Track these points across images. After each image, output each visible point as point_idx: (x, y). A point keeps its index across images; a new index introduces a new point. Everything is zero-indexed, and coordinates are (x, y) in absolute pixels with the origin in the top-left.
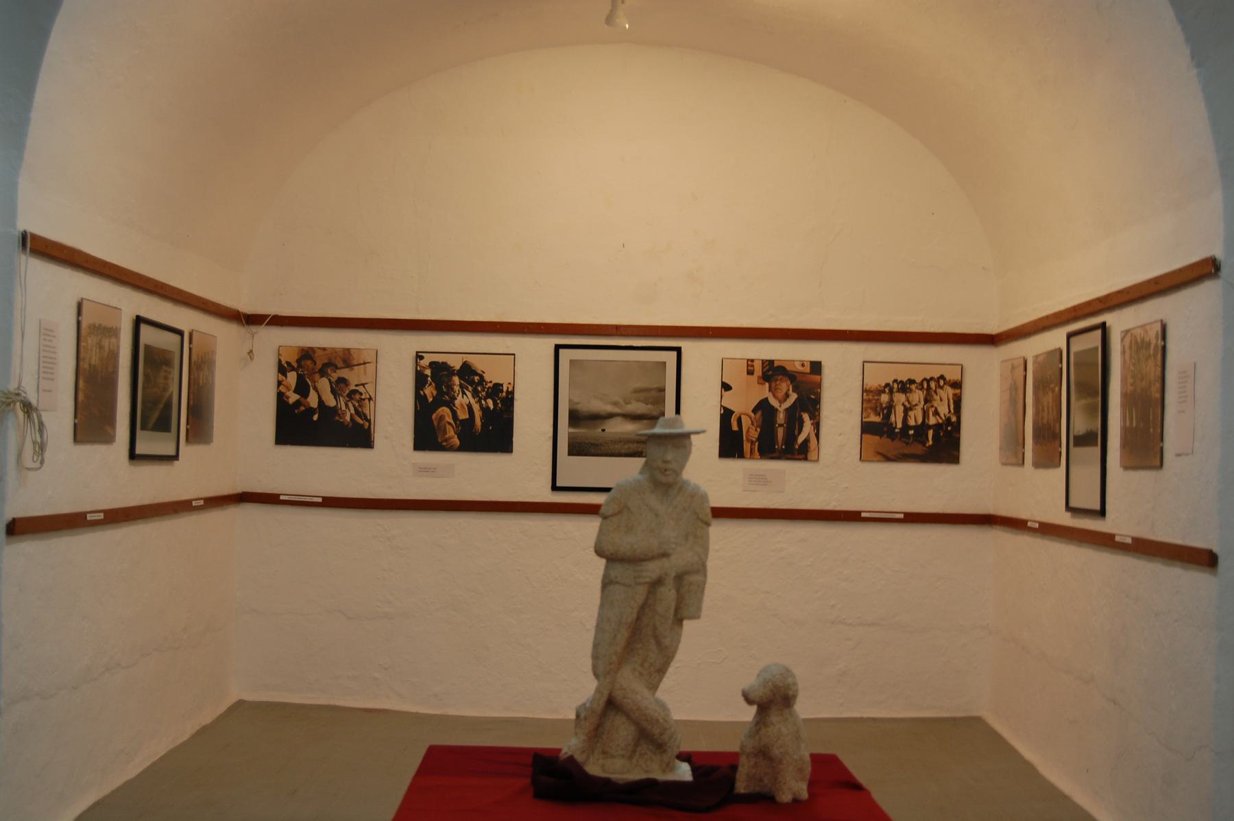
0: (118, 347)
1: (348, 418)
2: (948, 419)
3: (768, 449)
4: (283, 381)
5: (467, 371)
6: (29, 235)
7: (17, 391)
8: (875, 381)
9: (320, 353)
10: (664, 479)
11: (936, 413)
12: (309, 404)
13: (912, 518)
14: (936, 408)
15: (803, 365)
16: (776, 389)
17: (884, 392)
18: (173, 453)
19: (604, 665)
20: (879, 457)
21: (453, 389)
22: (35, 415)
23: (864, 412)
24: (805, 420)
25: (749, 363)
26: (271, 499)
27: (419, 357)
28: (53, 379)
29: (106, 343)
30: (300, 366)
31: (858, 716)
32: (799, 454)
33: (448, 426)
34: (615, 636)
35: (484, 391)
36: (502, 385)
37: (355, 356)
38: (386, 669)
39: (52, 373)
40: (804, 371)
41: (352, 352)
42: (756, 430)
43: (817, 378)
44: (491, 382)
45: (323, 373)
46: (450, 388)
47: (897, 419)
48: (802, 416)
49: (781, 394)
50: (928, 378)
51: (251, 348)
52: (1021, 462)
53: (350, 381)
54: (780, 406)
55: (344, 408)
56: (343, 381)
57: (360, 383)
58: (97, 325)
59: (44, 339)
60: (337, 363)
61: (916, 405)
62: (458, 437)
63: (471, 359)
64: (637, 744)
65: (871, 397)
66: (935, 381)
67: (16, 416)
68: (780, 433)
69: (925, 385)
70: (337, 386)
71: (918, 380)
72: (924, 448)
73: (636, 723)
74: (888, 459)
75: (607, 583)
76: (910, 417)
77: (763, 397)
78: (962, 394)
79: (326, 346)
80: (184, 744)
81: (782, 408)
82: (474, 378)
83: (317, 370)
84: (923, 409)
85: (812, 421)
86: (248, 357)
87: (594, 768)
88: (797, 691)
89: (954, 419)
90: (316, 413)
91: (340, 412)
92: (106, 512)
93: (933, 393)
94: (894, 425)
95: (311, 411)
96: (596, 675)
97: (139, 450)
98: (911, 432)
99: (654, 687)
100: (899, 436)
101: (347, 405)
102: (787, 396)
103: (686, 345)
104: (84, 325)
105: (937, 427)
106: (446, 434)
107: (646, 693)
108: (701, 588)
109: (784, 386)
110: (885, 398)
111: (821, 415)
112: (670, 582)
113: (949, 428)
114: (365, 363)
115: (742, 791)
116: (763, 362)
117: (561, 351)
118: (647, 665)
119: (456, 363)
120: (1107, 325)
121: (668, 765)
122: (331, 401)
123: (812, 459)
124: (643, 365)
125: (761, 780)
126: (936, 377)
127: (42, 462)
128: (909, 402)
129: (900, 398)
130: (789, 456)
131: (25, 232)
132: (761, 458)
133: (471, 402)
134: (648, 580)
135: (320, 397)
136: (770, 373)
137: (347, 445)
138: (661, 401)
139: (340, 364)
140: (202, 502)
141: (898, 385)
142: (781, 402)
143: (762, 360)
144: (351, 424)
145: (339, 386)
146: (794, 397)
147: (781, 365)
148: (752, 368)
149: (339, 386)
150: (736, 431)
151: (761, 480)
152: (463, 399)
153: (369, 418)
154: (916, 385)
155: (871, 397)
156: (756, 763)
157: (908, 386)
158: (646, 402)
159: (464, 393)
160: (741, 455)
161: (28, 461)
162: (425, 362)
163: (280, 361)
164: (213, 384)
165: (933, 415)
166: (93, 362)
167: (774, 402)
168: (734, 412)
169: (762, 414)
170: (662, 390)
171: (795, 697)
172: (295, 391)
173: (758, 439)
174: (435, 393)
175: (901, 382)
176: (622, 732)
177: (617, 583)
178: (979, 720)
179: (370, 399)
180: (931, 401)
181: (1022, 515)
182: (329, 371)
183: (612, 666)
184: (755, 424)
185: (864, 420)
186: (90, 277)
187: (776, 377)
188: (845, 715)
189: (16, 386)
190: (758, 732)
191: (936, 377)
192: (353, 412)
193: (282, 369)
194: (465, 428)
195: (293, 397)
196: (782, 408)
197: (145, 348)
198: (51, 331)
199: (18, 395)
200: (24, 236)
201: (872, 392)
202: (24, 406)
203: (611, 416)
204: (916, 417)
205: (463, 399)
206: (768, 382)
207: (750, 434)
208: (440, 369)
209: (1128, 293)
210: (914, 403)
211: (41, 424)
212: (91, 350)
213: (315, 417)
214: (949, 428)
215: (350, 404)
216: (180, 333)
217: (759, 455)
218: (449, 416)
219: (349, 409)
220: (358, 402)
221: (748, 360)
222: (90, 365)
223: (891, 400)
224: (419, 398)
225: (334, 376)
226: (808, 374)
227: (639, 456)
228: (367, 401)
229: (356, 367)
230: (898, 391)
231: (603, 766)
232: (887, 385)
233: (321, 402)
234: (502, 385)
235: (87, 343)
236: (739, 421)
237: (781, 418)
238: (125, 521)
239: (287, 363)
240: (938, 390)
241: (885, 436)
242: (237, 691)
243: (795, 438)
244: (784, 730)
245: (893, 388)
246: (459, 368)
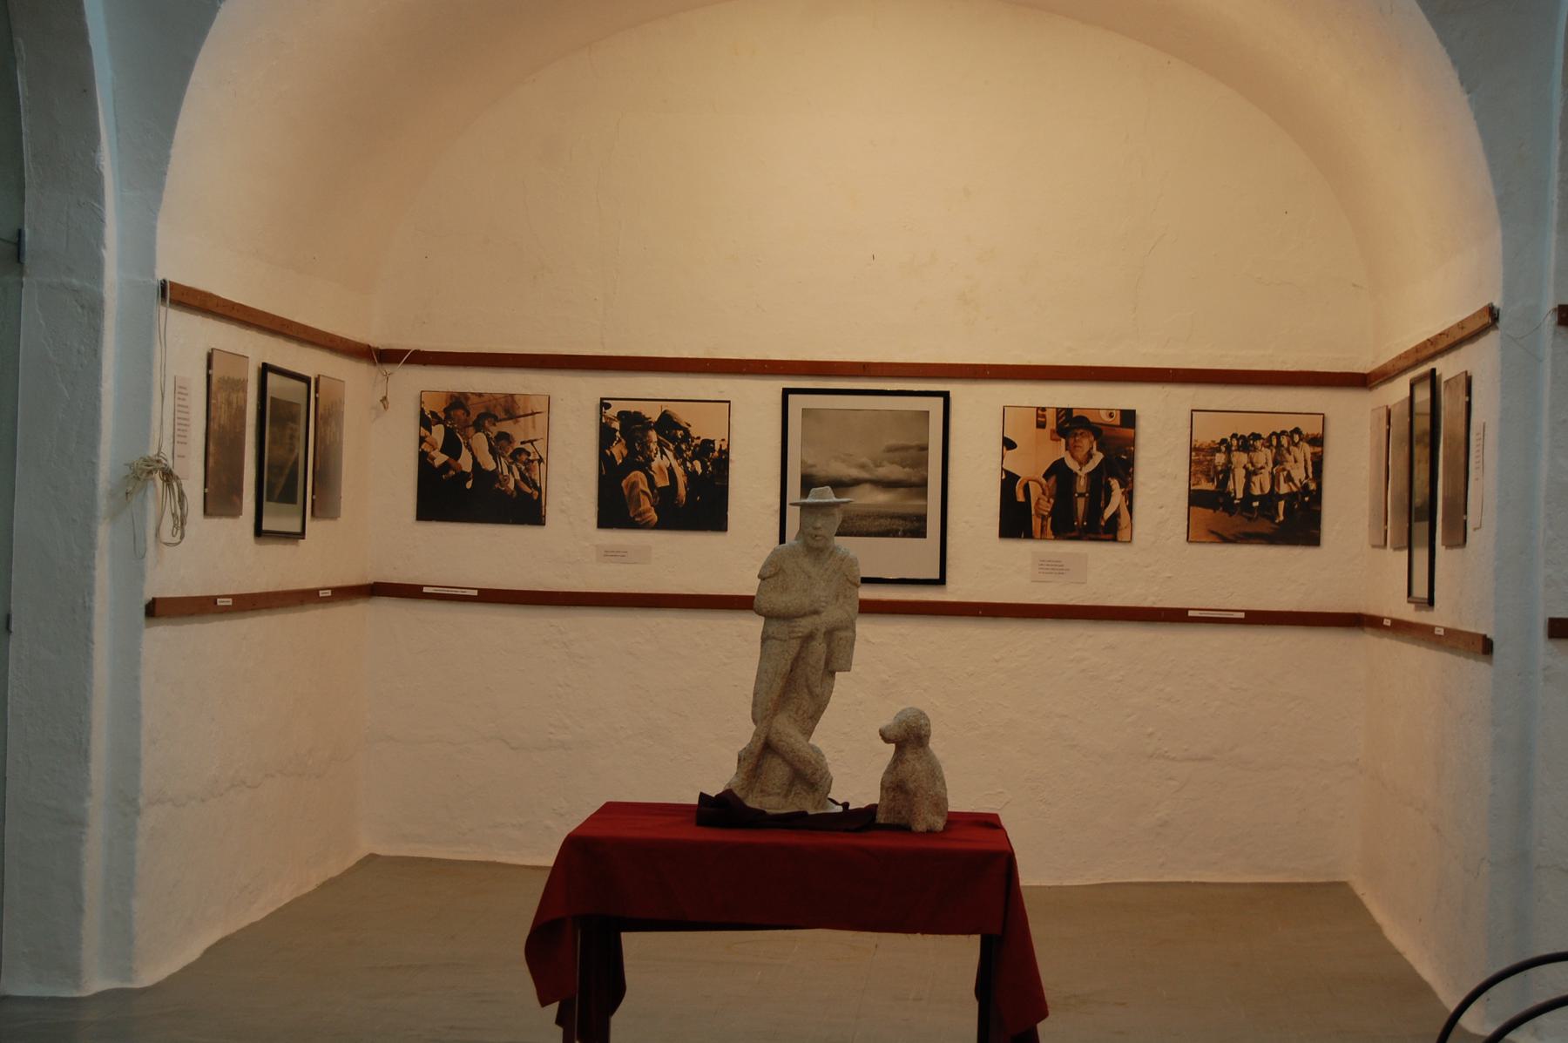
0: (245, 401)
1: (511, 485)
2: (1305, 487)
3: (1065, 526)
4: (426, 437)
5: (667, 424)
6: (168, 284)
7: (157, 458)
8: (1206, 437)
9: (474, 400)
10: (816, 544)
11: (1289, 479)
12: (461, 467)
13: (1256, 618)
14: (1289, 472)
15: (1111, 415)
16: (1075, 447)
17: (1219, 451)
18: (298, 529)
19: (764, 711)
20: (1212, 537)
21: (649, 448)
22: (175, 484)
23: (1192, 477)
24: (1113, 487)
25: (1039, 412)
27: (604, 404)
28: (185, 443)
29: (234, 397)
30: (448, 417)
31: (1185, 880)
32: (1105, 533)
33: (642, 496)
34: (772, 685)
35: (689, 449)
36: (713, 442)
37: (521, 404)
38: (562, 815)
39: (185, 436)
40: (1112, 423)
41: (517, 398)
42: (1049, 502)
43: (1128, 432)
44: (699, 438)
45: (479, 426)
46: (645, 445)
47: (1237, 486)
48: (1109, 482)
49: (1081, 454)
50: (1278, 432)
51: (385, 395)
52: (1383, 543)
53: (514, 436)
54: (1080, 470)
55: (506, 472)
56: (505, 437)
57: (527, 440)
58: (226, 378)
59: (179, 399)
60: (497, 414)
61: (1262, 468)
62: (656, 512)
63: (672, 408)
64: (792, 784)
66: (1287, 436)
67: (155, 486)
68: (1081, 504)
69: (1274, 442)
70: (496, 444)
71: (1265, 435)
72: (1273, 526)
73: (790, 764)
74: (1224, 540)
75: (765, 638)
76: (1254, 484)
77: (1059, 458)
78: (1325, 454)
79: (483, 392)
80: (308, 895)
81: (1083, 472)
82: (676, 433)
83: (471, 423)
84: (1272, 473)
85: (1123, 490)
86: (381, 404)
87: (752, 802)
88: (929, 731)
89: (1313, 486)
90: (470, 479)
91: (501, 477)
93: (1285, 452)
94: (1233, 495)
95: (463, 476)
96: (755, 721)
97: (267, 525)
98: (1256, 504)
99: (808, 733)
100: (1239, 509)
101: (510, 470)
102: (1090, 456)
103: (956, 389)
104: (214, 380)
105: (1291, 497)
106: (640, 506)
107: (801, 738)
108: (851, 643)
109: (1086, 443)
110: (1220, 459)
111: (1135, 481)
112: (820, 637)
113: (1307, 499)
114: (533, 414)
115: (882, 822)
116: (1059, 410)
117: (791, 397)
118: (801, 712)
119: (653, 413)
120: (1437, 373)
121: (819, 802)
122: (490, 465)
123: (1124, 540)
124: (898, 415)
125: (900, 813)
126: (1289, 431)
127: (182, 537)
128: (1253, 465)
129: (1240, 459)
130: (1093, 536)
131: (164, 281)
132: (1055, 539)
133: (673, 465)
134: (800, 634)
135: (474, 458)
136: (1067, 425)
137: (511, 521)
138: (923, 463)
139: (502, 415)
140: (329, 593)
141: (1238, 440)
142: (1082, 464)
143: (1057, 409)
144: (515, 494)
145: (499, 444)
146: (1098, 457)
147: (1084, 415)
148: (1043, 420)
149: (499, 444)
150: (1021, 502)
151: (1055, 568)
152: (663, 461)
153: (538, 485)
154: (1262, 441)
155: (1201, 457)
156: (894, 797)
157: (1251, 442)
158: (903, 464)
159: (663, 453)
160: (1029, 535)
161: (166, 535)
162: (612, 412)
163: (422, 411)
164: (341, 443)
165: (1285, 482)
166: (222, 422)
167: (1072, 464)
168: (1019, 478)
169: (1057, 481)
170: (924, 448)
171: (927, 736)
172: (442, 451)
173: (1051, 514)
174: (625, 452)
175: (1242, 437)
176: (778, 772)
177: (774, 638)
178: (1344, 884)
179: (540, 460)
180: (1281, 463)
181: (1372, 610)
182: (487, 424)
183: (768, 712)
184: (1047, 493)
185: (1192, 488)
186: (219, 323)
187: (1076, 431)
188: (1166, 879)
189: (155, 452)
190: (895, 768)
191: (1289, 431)
192: (518, 477)
193: (426, 422)
194: (664, 499)
195: (440, 459)
196: (1083, 472)
197: (271, 401)
198: (185, 388)
199: (158, 461)
200: (164, 285)
201: (1203, 450)
202: (163, 474)
203: (856, 482)
204: (1261, 484)
205: (663, 461)
206: (1065, 438)
207: (1041, 507)
208: (633, 423)
209: (1447, 336)
210: (1259, 466)
211: (182, 495)
212: (221, 408)
213: (469, 485)
214: (1307, 499)
215: (514, 466)
216: (306, 380)
217: (1054, 534)
218: (644, 484)
219: (513, 474)
220: (525, 464)
221: (1038, 408)
222: (219, 426)
223: (1229, 461)
224: (605, 459)
225: (494, 431)
226: (1117, 426)
227: (894, 536)
228: (536, 463)
229: (522, 419)
230: (1238, 450)
231: (761, 802)
232: (1223, 441)
233: (476, 464)
234: (713, 442)
235: (217, 400)
236: (1026, 489)
237: (1082, 485)
238: (252, 610)
239: (432, 413)
240: (1292, 448)
241: (1221, 509)
242: (368, 844)
243: (1100, 512)
244: (918, 766)
245: (1232, 445)
246: (656, 420)
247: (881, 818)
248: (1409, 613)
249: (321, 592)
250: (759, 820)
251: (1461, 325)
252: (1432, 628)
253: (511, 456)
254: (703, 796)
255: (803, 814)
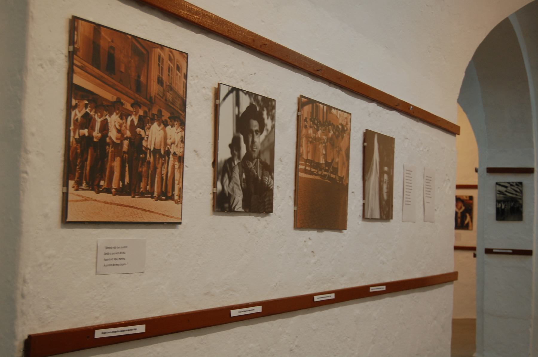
43: (471, 202)
49: (459, 207)
65: (142, 190)
68: (127, 169)
102: (461, 208)
146: (463, 208)
249: (371, 288)
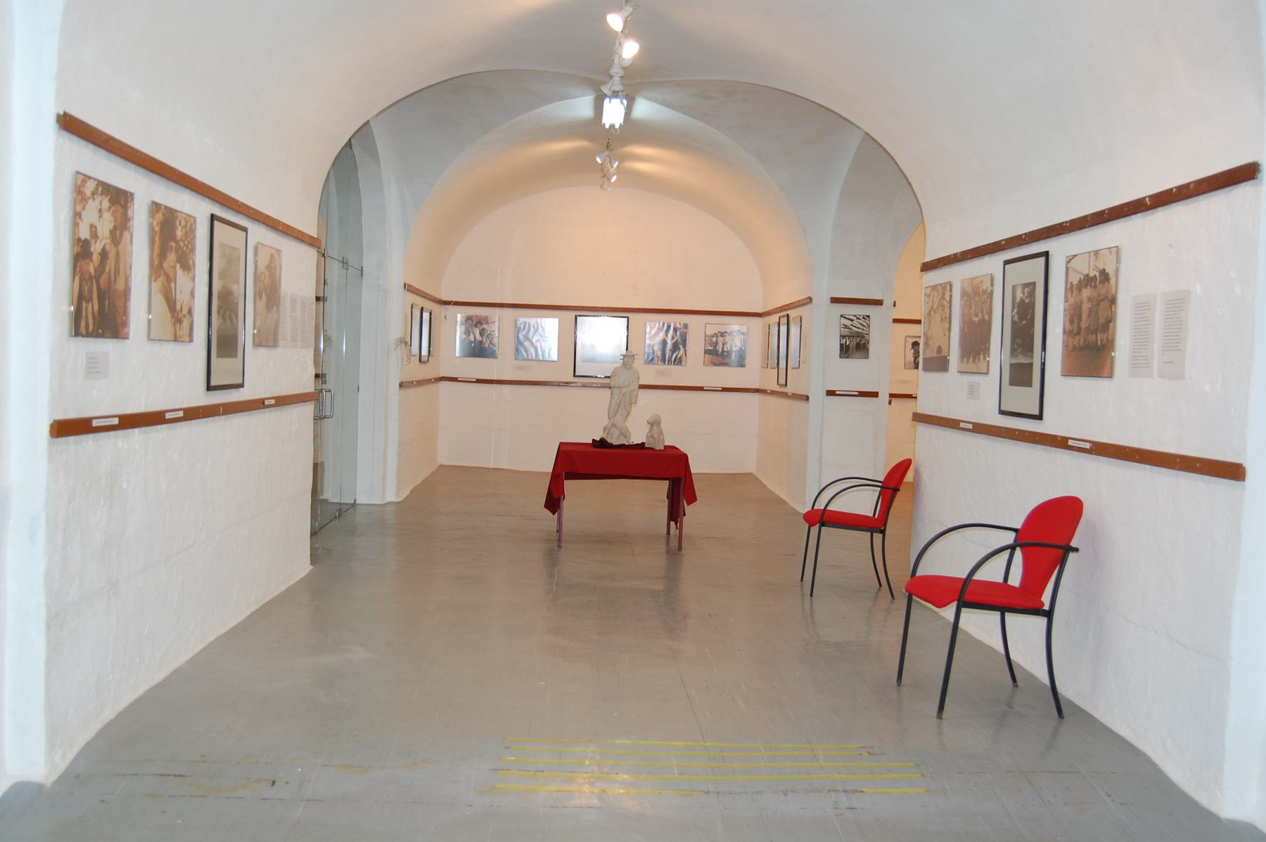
1: (487, 345)
11: (735, 346)
26: (455, 379)
45: (476, 326)
47: (719, 348)
92: (185, 410)
110: (714, 339)
129: (720, 339)
178: (751, 473)
223: (717, 340)
225: (481, 327)
232: (715, 334)
247: (646, 446)
248: (777, 388)
250: (611, 446)
251: (799, 301)
252: (787, 393)
253: (487, 336)
254: (593, 440)
255: (624, 445)
